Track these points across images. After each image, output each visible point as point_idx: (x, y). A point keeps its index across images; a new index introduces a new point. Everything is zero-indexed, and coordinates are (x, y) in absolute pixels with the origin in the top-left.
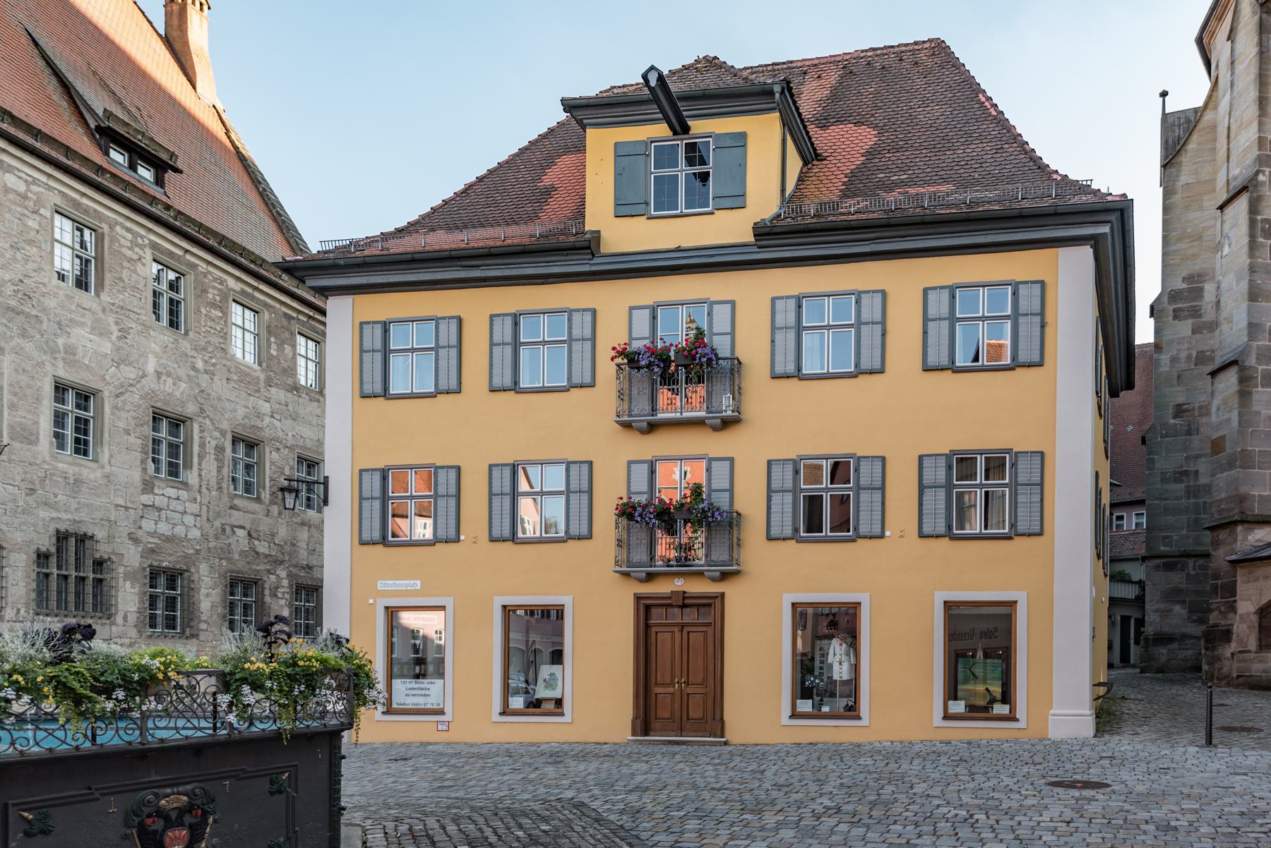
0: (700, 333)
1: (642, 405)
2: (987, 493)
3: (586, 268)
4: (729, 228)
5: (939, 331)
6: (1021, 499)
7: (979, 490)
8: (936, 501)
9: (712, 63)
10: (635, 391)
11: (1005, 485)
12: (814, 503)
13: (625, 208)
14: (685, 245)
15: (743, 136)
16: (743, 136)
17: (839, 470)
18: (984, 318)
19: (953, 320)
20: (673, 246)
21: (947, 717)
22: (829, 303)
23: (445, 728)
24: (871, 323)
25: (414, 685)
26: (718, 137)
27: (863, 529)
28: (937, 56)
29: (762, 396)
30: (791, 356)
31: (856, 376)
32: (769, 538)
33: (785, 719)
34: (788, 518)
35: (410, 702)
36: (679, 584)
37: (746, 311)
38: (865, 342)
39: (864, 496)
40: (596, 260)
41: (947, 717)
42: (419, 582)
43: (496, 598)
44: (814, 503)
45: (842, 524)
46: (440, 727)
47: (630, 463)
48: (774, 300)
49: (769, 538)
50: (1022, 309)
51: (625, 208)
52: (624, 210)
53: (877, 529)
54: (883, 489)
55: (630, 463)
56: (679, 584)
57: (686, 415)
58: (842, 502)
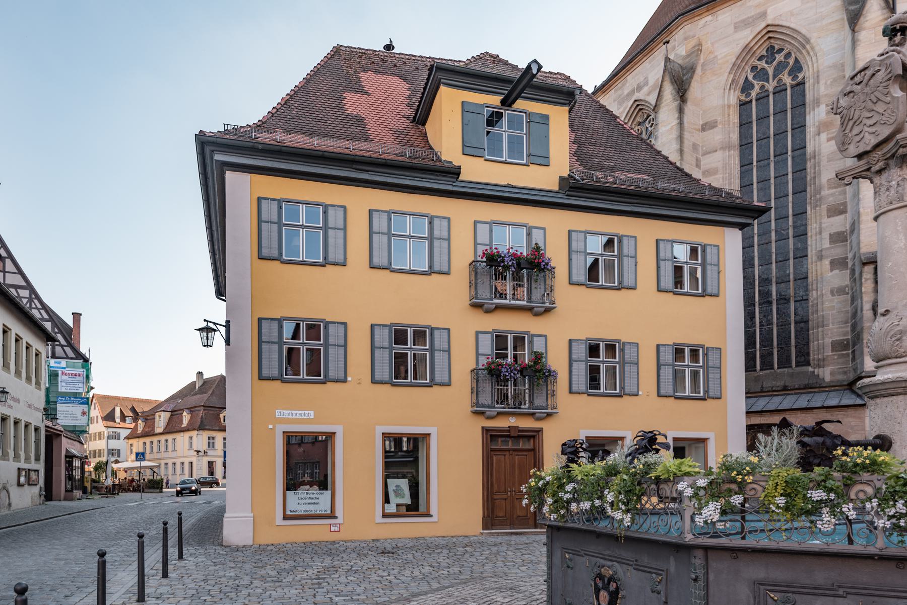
0: (537, 249)
1: (485, 292)
2: (414, 354)
3: (450, 188)
4: (545, 178)
5: (269, 231)
6: (711, 376)
7: (407, 355)
8: (667, 374)
9: (496, 59)
10: (479, 281)
11: (701, 367)
12: (292, 353)
13: (542, 159)
14: (515, 184)
15: (546, 117)
16: (546, 117)
17: (314, 329)
18: (302, 227)
19: (389, 235)
20: (505, 183)
21: (385, 515)
22: (302, 209)
23: (337, 529)
24: (328, 225)
25: (305, 496)
26: (529, 114)
27: (332, 374)
28: (337, 51)
29: (566, 295)
30: (275, 245)
31: (430, 275)
32: (571, 392)
33: (379, 518)
34: (276, 364)
35: (302, 509)
36: (512, 421)
37: (559, 234)
38: (331, 241)
39: (331, 351)
40: (457, 184)
41: (385, 515)
42: (312, 413)
43: (341, 427)
44: (292, 353)
45: (314, 369)
46: (333, 529)
47: (477, 333)
48: (476, 223)
49: (571, 392)
50: (331, 224)
51: (542, 159)
52: (468, 151)
53: (341, 375)
54: (345, 346)
55: (477, 333)
56: (512, 421)
57: (513, 302)
58: (313, 354)
